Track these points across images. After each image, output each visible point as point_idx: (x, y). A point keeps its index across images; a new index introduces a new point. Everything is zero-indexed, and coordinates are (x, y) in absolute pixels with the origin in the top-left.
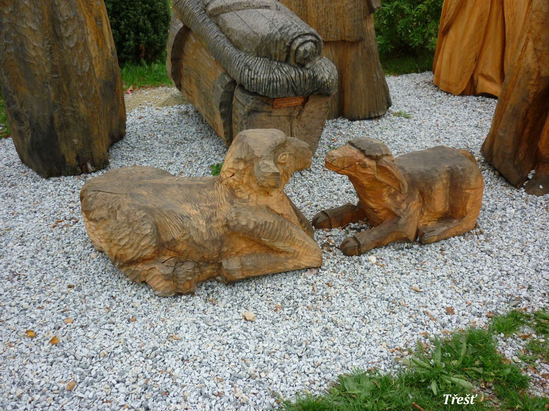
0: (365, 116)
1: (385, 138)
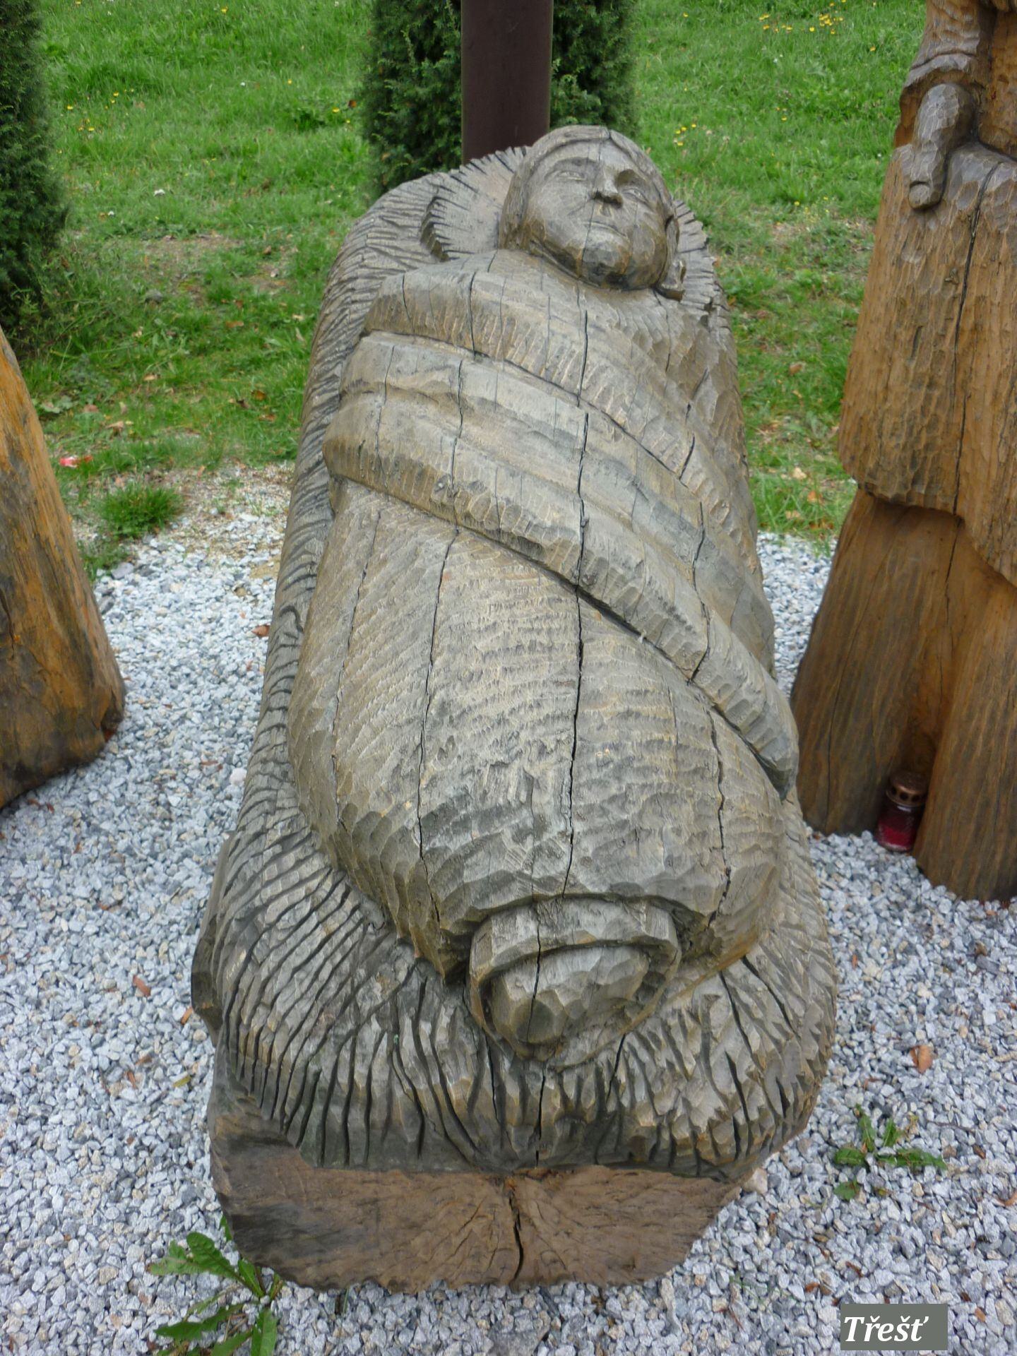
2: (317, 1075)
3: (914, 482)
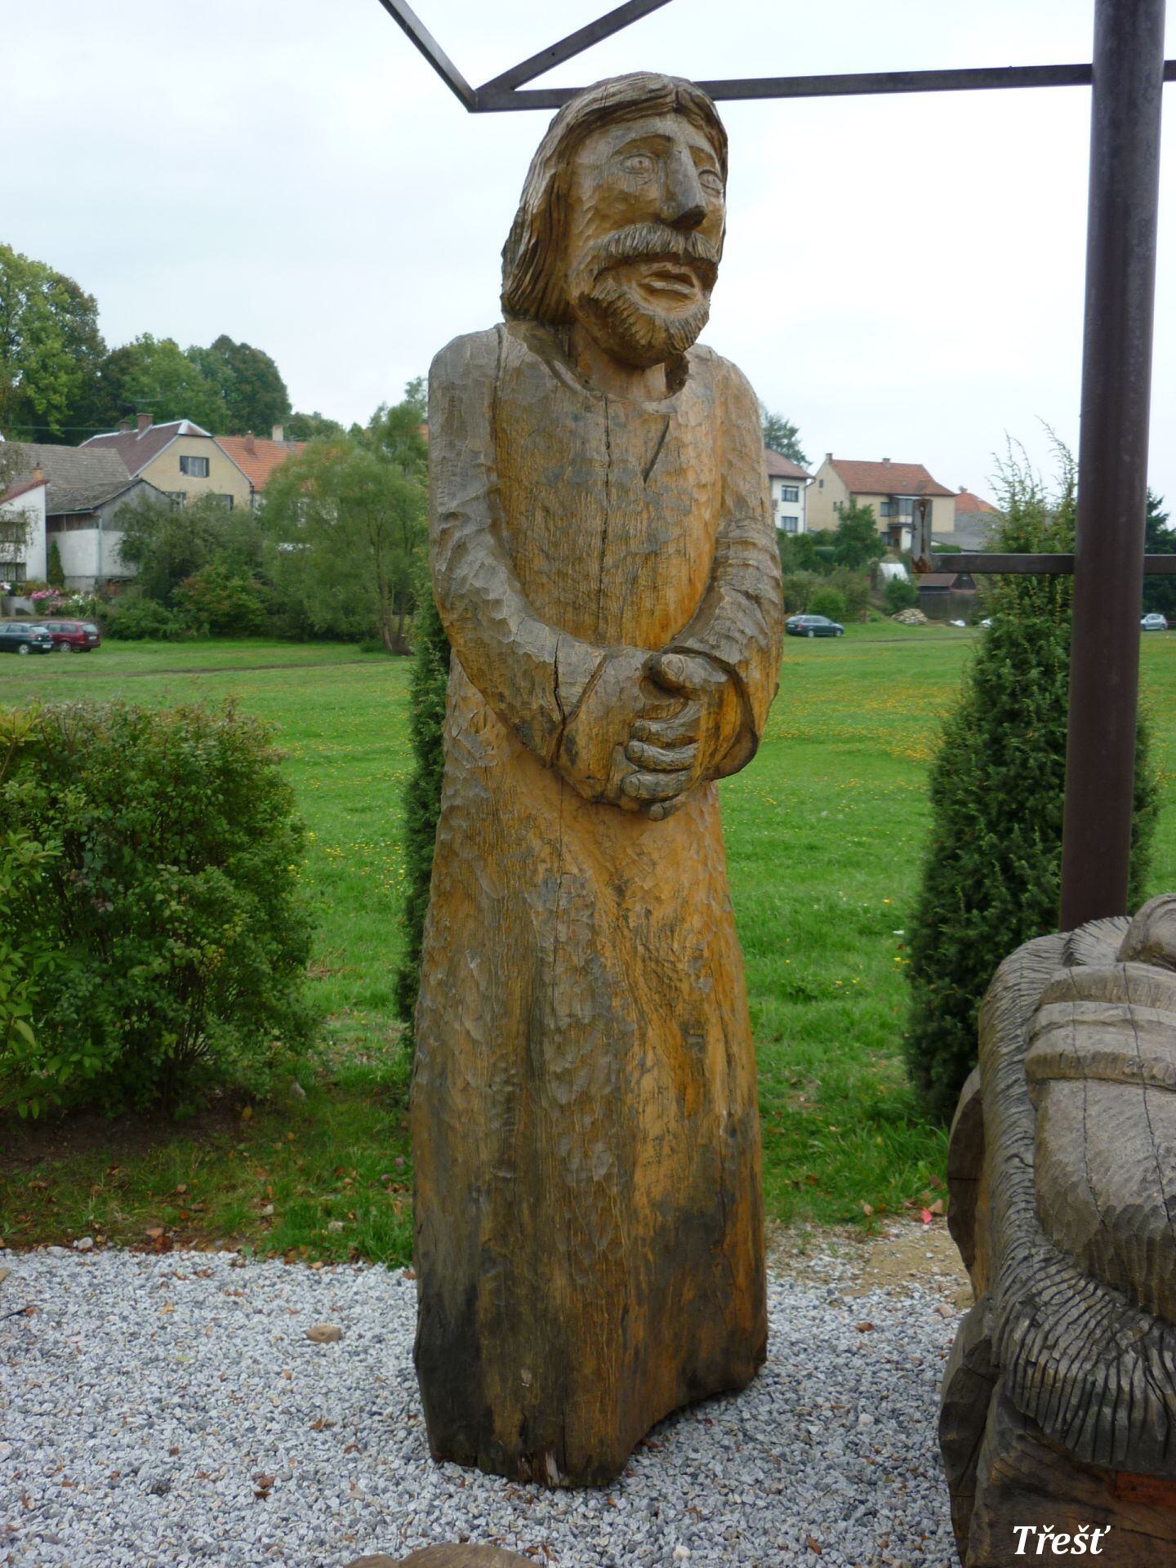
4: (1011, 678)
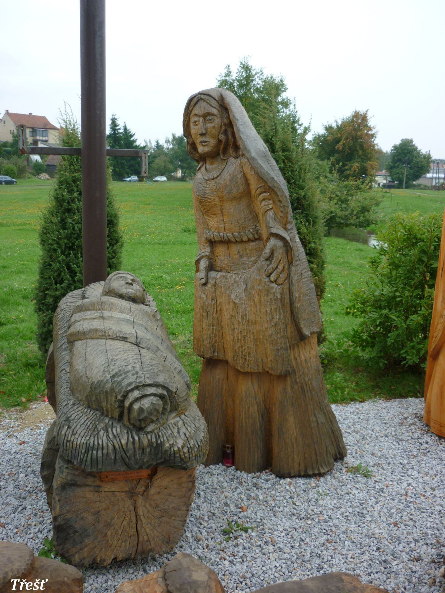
0: (300, 472)
1: (318, 511)
2: (89, 444)
3: (214, 352)
4: (67, 196)
